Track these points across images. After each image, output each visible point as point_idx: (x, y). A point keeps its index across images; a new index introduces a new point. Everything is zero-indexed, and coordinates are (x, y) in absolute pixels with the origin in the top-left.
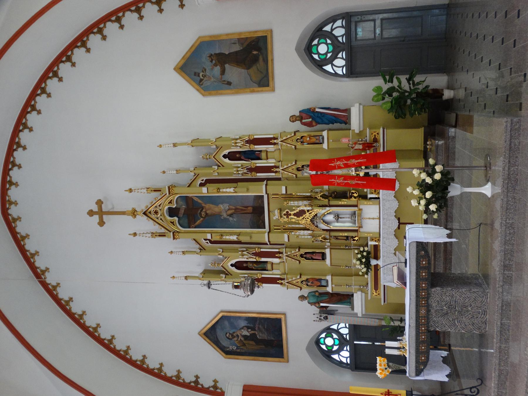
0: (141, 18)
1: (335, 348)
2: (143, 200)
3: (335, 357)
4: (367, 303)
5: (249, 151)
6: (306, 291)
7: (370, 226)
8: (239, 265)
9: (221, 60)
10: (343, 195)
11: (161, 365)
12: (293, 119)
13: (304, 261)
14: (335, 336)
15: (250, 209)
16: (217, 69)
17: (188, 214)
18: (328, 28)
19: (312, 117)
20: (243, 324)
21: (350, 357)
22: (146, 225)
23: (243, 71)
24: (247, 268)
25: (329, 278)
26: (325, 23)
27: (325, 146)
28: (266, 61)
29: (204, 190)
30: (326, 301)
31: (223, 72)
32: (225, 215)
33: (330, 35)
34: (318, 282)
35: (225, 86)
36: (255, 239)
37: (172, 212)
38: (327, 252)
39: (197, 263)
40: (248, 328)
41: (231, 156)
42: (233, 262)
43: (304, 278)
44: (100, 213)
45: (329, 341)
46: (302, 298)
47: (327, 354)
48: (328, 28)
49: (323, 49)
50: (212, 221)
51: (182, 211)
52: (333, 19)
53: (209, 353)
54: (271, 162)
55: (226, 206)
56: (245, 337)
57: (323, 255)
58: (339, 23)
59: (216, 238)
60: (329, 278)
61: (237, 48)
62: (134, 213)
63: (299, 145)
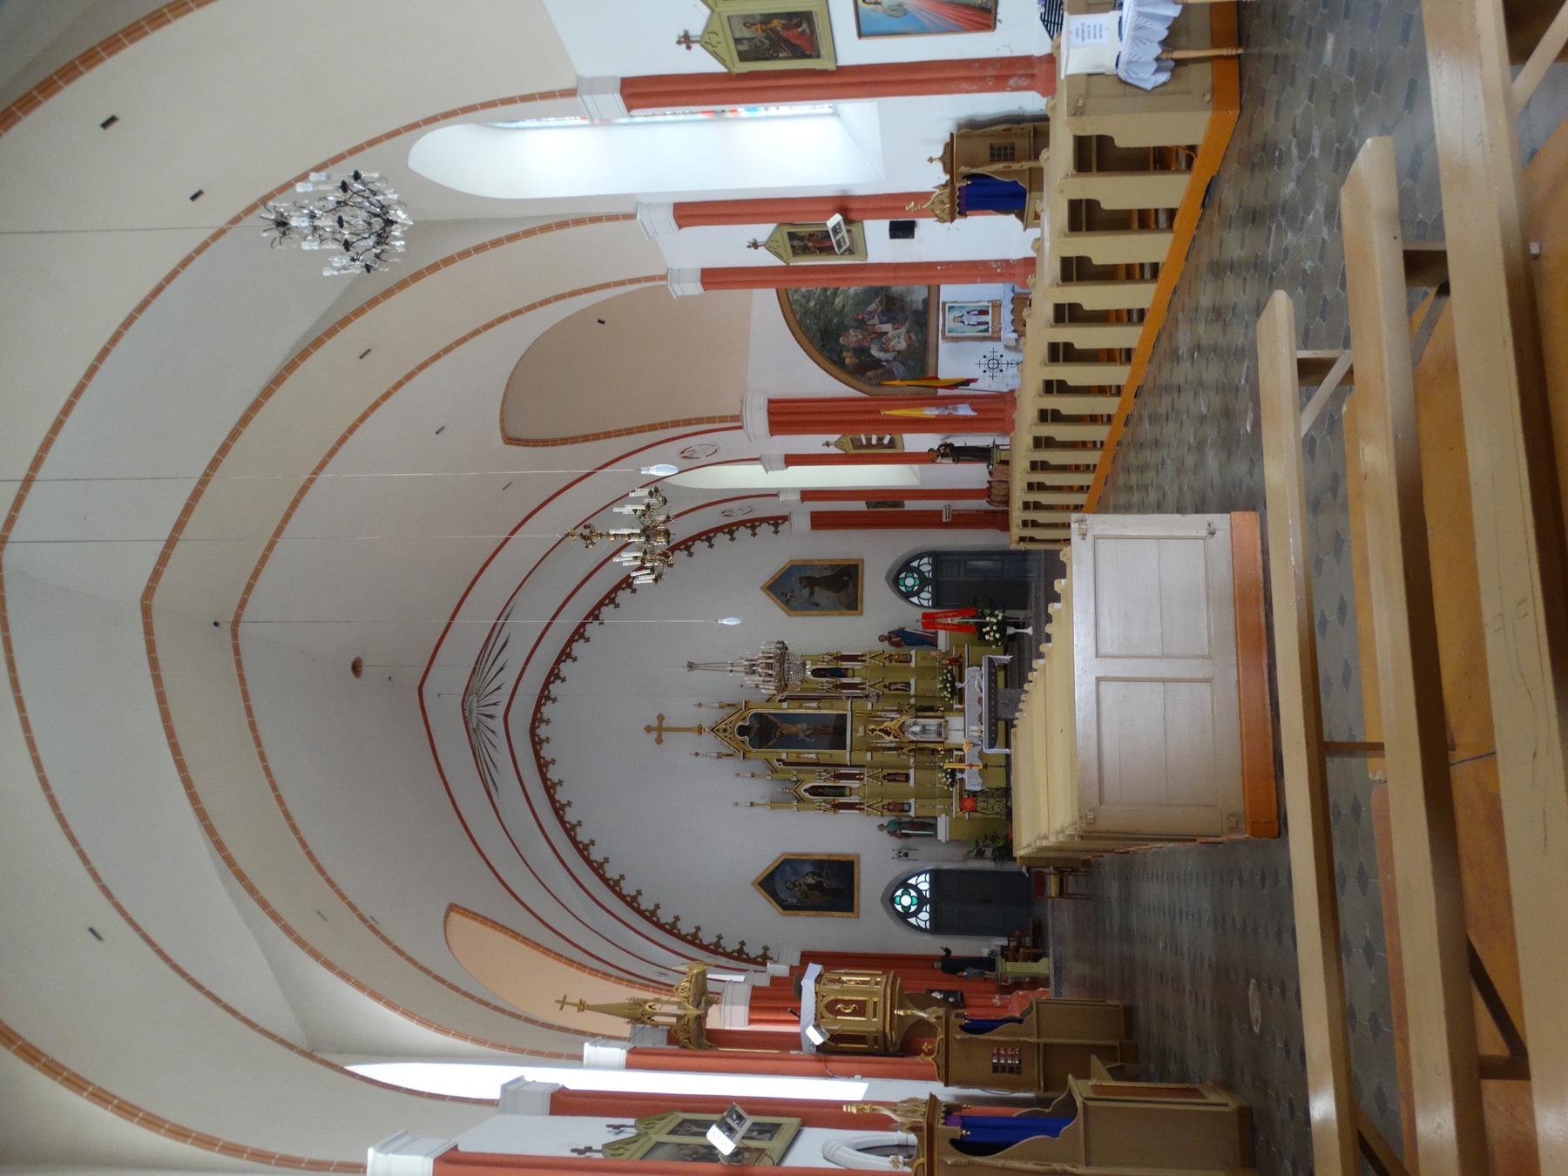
0: (776, 532)
1: (913, 908)
2: (709, 717)
3: (913, 920)
4: (952, 825)
5: (834, 670)
6: (885, 821)
7: (956, 738)
8: (814, 791)
9: (811, 582)
10: (931, 709)
11: (698, 928)
12: (882, 639)
13: (885, 782)
14: (913, 893)
15: (831, 730)
16: (806, 591)
17: (760, 732)
18: (915, 564)
19: (900, 638)
20: (808, 868)
21: (931, 919)
22: (709, 743)
23: (832, 595)
24: (821, 794)
25: (912, 801)
26: (913, 559)
27: (913, 664)
28: (856, 587)
29: (785, 705)
30: (909, 827)
31: (812, 594)
32: (802, 735)
33: (917, 570)
34: (901, 808)
35: (812, 606)
36: (835, 760)
37: (743, 731)
38: (912, 772)
39: (761, 789)
40: (814, 874)
41: (816, 673)
42: (807, 786)
43: (886, 802)
44: (659, 730)
45: (906, 901)
46: (881, 827)
47: (905, 915)
48: (915, 564)
49: (909, 582)
50: (789, 742)
51: (753, 732)
52: (920, 556)
53: (764, 907)
54: (857, 680)
55: (805, 726)
56: (809, 886)
57: (907, 777)
58: (925, 560)
59: (793, 758)
60: (912, 801)
61: (828, 573)
62: (700, 730)
63: (887, 663)
